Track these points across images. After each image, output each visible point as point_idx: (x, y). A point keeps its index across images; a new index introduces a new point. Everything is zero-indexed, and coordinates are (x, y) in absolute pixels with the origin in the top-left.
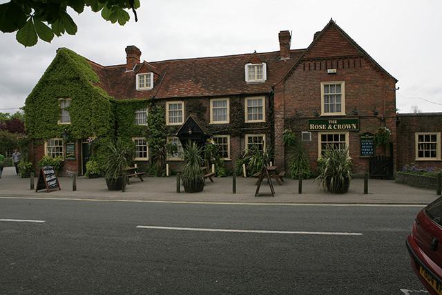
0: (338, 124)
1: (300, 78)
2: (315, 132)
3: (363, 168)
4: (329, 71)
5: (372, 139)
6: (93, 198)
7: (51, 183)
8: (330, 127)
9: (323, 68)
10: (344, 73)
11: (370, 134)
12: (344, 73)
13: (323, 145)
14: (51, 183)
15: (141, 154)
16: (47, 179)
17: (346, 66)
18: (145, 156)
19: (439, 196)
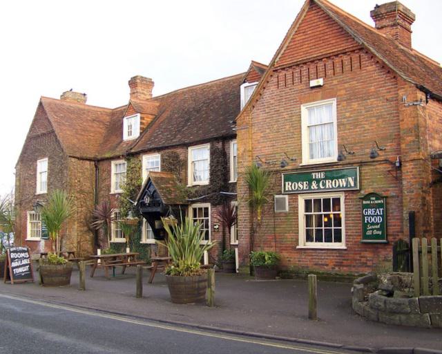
0: (326, 178)
1: (272, 101)
2: (294, 195)
3: (369, 263)
4: (313, 83)
5: (380, 206)
6: (10, 301)
7: (20, 270)
8: (314, 185)
9: (304, 79)
10: (335, 82)
11: (378, 197)
12: (335, 82)
13: (308, 218)
14: (20, 270)
15: (328, 232)
16: (14, 264)
17: (338, 70)
18: (338, 239)
19: (371, 23)
